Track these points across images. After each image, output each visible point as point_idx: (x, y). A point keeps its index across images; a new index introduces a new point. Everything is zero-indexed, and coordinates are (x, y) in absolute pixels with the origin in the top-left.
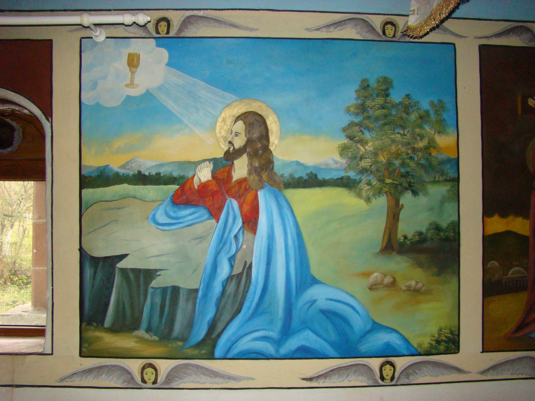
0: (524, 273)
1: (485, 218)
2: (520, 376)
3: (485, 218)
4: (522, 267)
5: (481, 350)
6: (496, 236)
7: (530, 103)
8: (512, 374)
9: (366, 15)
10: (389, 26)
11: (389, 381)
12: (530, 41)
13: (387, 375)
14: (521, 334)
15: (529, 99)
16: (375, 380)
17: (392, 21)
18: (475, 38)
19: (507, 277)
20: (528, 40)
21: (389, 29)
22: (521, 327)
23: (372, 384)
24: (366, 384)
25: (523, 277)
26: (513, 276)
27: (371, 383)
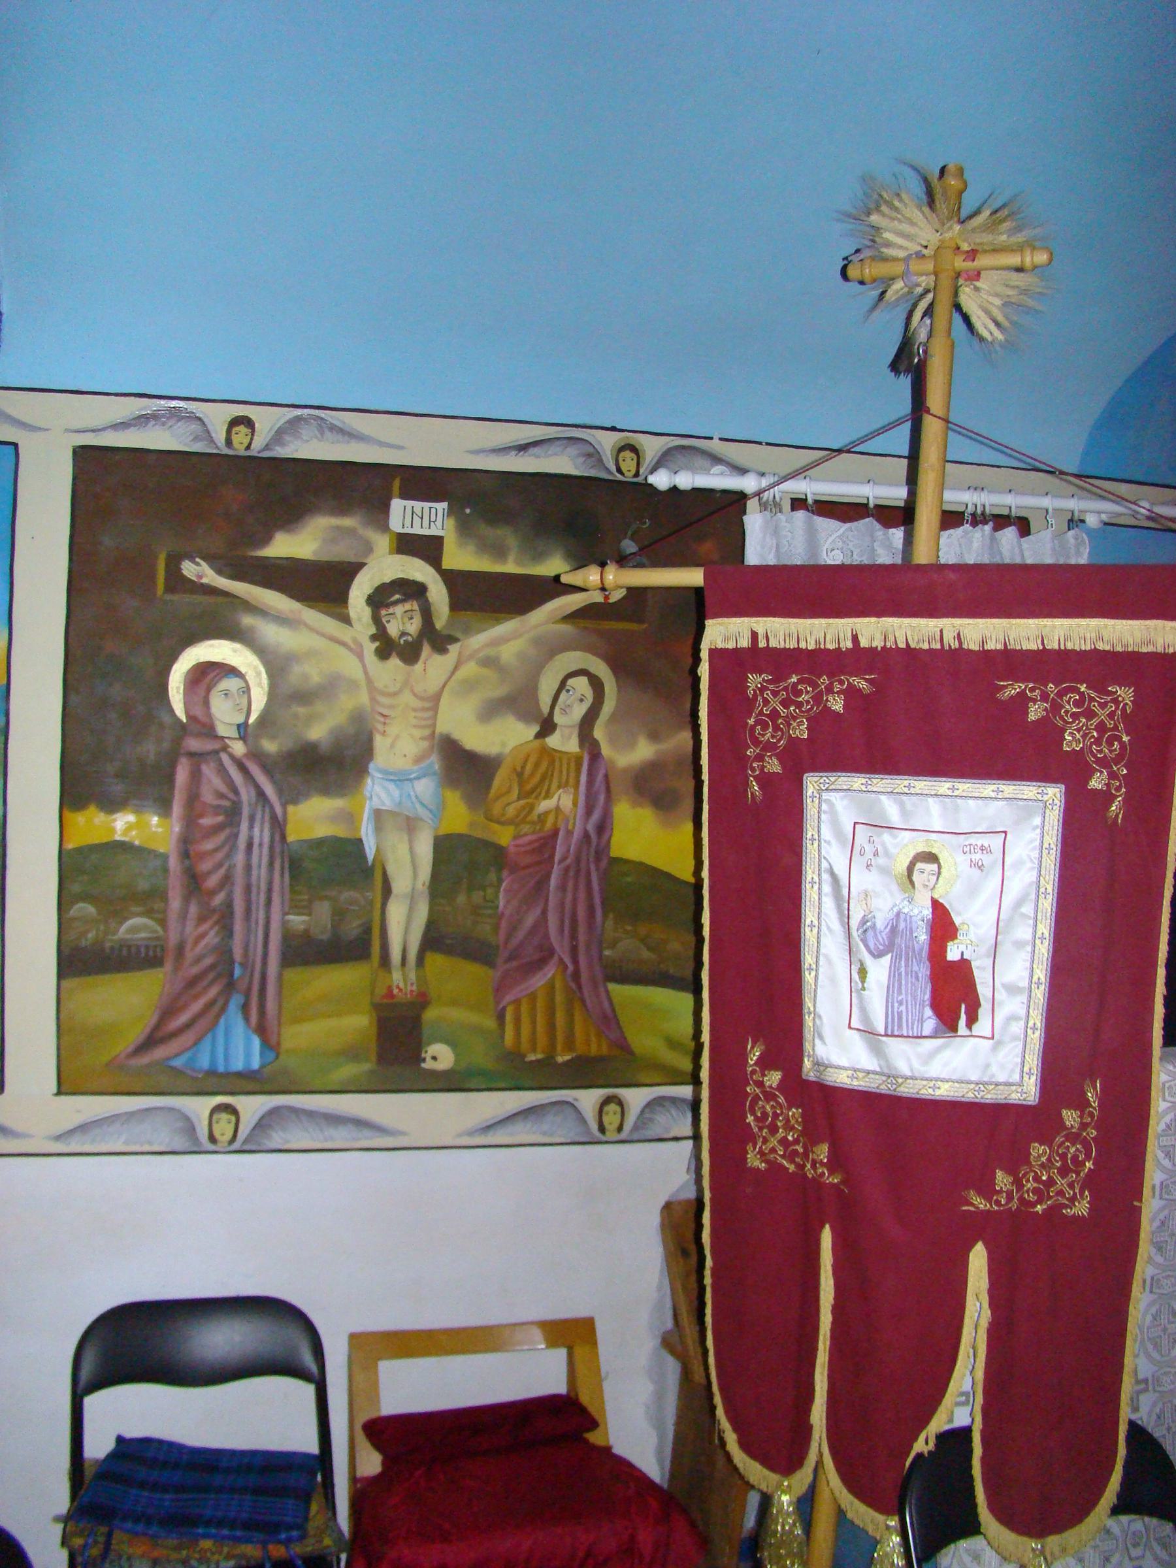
0: (156, 932)
1: (67, 814)
2: (146, 1148)
3: (67, 814)
4: (152, 918)
5: (55, 1090)
6: (85, 851)
7: (185, 572)
8: (126, 1143)
9: (589, 431)
10: (628, 454)
11: (226, 1144)
12: (196, 439)
13: (610, 1124)
14: (145, 1060)
15: (183, 563)
16: (588, 1131)
17: (632, 443)
18: (67, 430)
19: (115, 937)
20: (191, 438)
21: (242, 435)
22: (150, 1042)
23: (577, 1139)
24: (563, 1140)
25: (158, 938)
26: (129, 936)
27: (179, 1143)
